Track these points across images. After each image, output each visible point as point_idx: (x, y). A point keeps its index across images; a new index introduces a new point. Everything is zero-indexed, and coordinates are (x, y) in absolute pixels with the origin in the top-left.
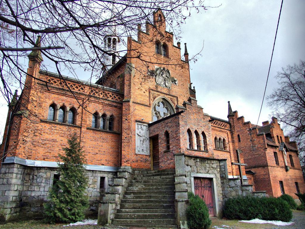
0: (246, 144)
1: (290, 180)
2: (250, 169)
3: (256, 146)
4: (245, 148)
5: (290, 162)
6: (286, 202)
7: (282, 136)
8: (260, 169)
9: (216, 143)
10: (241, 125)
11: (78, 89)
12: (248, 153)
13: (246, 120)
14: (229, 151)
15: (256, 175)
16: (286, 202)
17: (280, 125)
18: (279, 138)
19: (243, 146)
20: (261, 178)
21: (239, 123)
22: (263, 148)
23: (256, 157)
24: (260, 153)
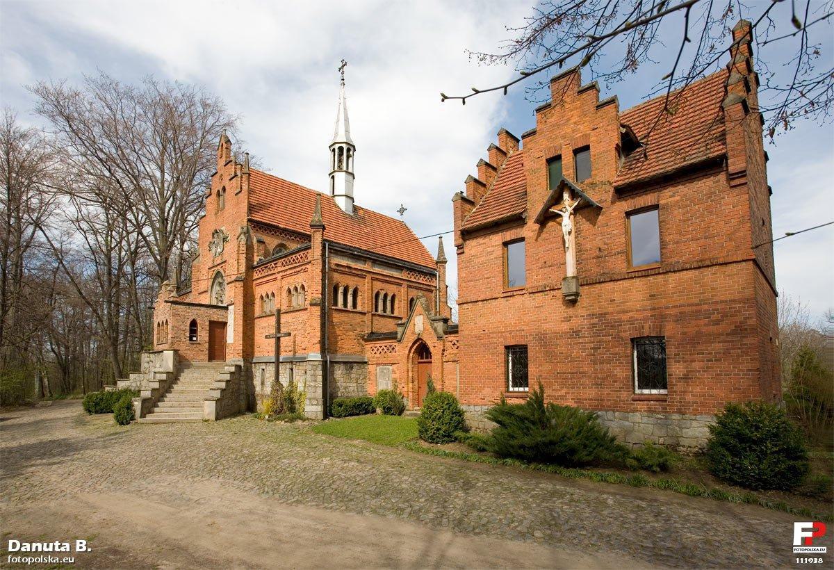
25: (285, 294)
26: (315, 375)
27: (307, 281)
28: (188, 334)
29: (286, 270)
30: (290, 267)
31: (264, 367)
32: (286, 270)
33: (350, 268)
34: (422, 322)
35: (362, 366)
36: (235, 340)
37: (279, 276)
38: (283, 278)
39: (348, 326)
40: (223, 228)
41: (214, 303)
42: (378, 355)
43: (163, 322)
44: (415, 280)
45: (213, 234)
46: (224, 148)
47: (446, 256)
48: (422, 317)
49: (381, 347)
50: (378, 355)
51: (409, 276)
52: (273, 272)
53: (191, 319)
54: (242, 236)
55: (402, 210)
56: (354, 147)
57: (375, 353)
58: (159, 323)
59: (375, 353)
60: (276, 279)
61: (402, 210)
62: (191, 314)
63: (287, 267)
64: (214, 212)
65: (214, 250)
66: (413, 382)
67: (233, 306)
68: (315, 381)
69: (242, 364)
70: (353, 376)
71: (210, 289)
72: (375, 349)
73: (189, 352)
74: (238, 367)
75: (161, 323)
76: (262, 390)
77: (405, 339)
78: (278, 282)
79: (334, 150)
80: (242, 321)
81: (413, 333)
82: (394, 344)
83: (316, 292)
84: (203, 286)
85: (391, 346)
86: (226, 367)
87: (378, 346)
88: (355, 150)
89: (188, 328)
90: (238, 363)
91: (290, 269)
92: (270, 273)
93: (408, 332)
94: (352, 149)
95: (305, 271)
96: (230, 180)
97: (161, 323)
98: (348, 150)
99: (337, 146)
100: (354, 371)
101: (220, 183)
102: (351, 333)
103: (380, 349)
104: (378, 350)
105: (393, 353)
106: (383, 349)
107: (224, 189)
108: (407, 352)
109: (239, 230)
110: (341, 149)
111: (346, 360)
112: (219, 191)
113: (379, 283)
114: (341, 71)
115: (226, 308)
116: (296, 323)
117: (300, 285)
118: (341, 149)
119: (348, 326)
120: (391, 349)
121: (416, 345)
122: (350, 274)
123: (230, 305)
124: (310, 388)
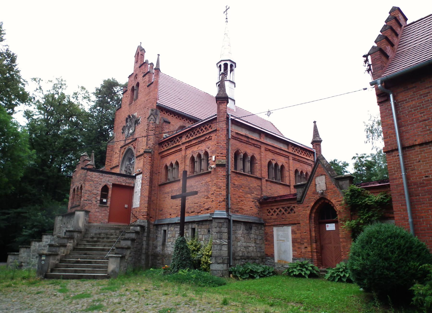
25: (188, 162)
26: (220, 232)
27: (211, 147)
28: (99, 198)
29: (191, 141)
30: (194, 137)
31: (166, 228)
32: (191, 141)
33: (248, 137)
34: (324, 181)
35: (260, 227)
36: (141, 204)
37: (183, 147)
38: (186, 148)
39: (247, 189)
40: (136, 114)
41: (123, 172)
42: (275, 216)
43: (78, 187)
44: (298, 154)
45: (127, 119)
46: (140, 54)
47: (321, 137)
48: (324, 177)
49: (277, 209)
50: (275, 216)
51: (294, 151)
52: (178, 144)
53: (103, 184)
54: (152, 117)
55: (269, 113)
56: (235, 63)
57: (272, 215)
58: (74, 190)
59: (272, 215)
60: (180, 150)
61: (269, 113)
62: (103, 180)
63: (191, 138)
64: (128, 103)
65: (126, 132)
66: (316, 242)
67: (141, 175)
68: (221, 238)
69: (146, 225)
70: (252, 236)
71: (120, 163)
72: (272, 212)
73: (98, 214)
74: (142, 227)
75: (76, 189)
76: (163, 250)
77: (306, 200)
78: (183, 152)
79: (220, 66)
80: (148, 187)
81: (315, 192)
82: (293, 205)
83: (221, 155)
84: (115, 162)
85: (289, 207)
86: (131, 228)
87: (275, 208)
88: (235, 67)
89: (99, 192)
90: (142, 224)
91: (194, 139)
92: (175, 145)
93: (309, 192)
94: (234, 65)
95: (210, 139)
96: (143, 76)
97: (76, 189)
98: (231, 66)
99: (222, 63)
100: (253, 231)
101: (135, 80)
102: (249, 195)
103: (278, 211)
104: (275, 212)
105: (292, 214)
106: (280, 211)
107: (138, 85)
108: (309, 212)
109: (150, 112)
110: (226, 65)
111: (246, 220)
112: (133, 87)
113: (270, 154)
114: (225, 13)
115: (134, 177)
116: (198, 186)
117: (204, 151)
118: (226, 65)
119: (247, 189)
120: (289, 210)
121: (318, 205)
122: (247, 143)
123: (138, 174)
124: (216, 246)
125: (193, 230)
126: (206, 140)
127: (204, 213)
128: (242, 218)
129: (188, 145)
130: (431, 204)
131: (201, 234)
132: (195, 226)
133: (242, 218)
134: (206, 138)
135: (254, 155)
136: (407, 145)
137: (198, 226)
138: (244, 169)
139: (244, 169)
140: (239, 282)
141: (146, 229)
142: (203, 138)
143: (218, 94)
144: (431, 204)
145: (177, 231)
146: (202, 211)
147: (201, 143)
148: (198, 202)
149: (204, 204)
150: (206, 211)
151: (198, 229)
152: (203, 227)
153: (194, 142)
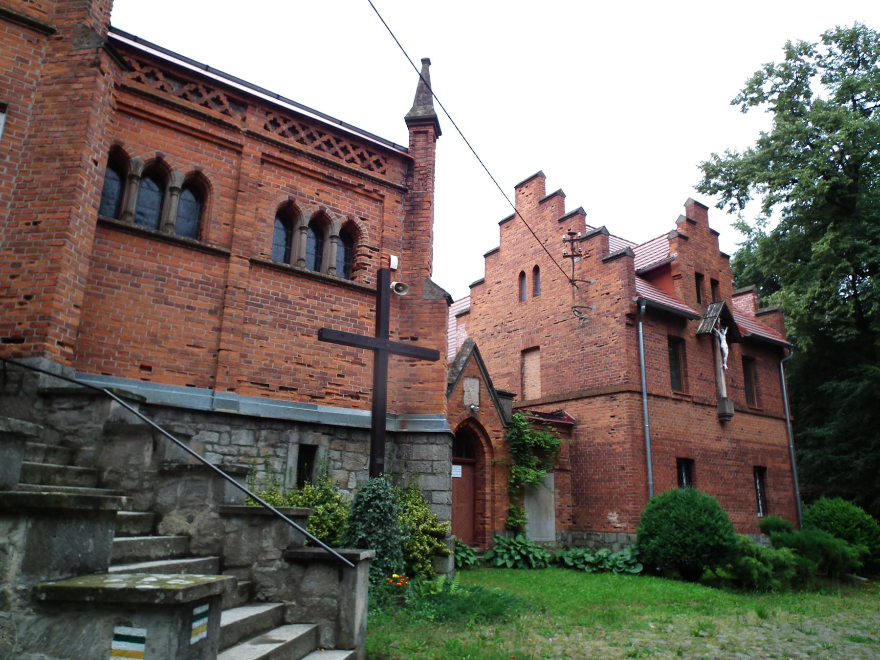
0: (558, 302)
1: (730, 456)
2: (561, 406)
3: (594, 307)
4: (551, 317)
5: (742, 385)
6: (472, 426)
7: (720, 279)
8: (598, 402)
9: (765, 413)
10: (550, 224)
11: (279, 130)
12: (560, 338)
13: (593, 221)
14: (372, 285)
15: (579, 427)
16: (472, 426)
17: (717, 234)
18: (707, 284)
19: (547, 313)
20: (599, 444)
21: (543, 219)
22: (618, 315)
23: (587, 355)
24: (605, 335)
117: (344, 218)
125: (307, 454)
126: (359, 190)
127: (341, 403)
128: (296, 411)
129: (277, 154)
130: (4, 293)
131: (341, 468)
132: (323, 442)
133: (296, 411)
134: (360, 186)
135: (298, 203)
136: (636, 396)
137: (330, 441)
138: (318, 262)
139: (318, 262)
140: (531, 572)
141: (868, 517)
142: (351, 180)
143: (412, 110)
144: (4, 293)
145: (212, 443)
146: (327, 393)
147: (334, 185)
148: (317, 363)
149: (343, 376)
150: (350, 398)
151: (328, 451)
152: (351, 446)
153: (311, 166)
